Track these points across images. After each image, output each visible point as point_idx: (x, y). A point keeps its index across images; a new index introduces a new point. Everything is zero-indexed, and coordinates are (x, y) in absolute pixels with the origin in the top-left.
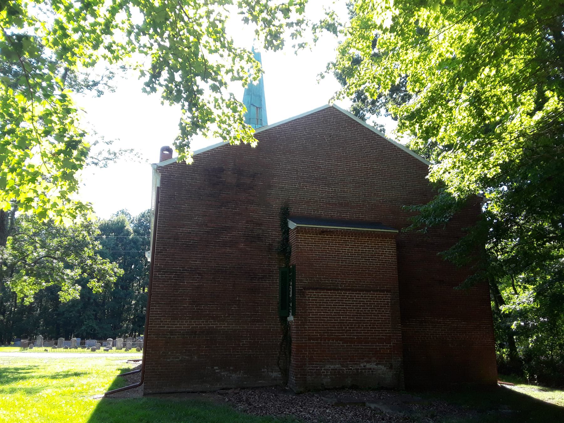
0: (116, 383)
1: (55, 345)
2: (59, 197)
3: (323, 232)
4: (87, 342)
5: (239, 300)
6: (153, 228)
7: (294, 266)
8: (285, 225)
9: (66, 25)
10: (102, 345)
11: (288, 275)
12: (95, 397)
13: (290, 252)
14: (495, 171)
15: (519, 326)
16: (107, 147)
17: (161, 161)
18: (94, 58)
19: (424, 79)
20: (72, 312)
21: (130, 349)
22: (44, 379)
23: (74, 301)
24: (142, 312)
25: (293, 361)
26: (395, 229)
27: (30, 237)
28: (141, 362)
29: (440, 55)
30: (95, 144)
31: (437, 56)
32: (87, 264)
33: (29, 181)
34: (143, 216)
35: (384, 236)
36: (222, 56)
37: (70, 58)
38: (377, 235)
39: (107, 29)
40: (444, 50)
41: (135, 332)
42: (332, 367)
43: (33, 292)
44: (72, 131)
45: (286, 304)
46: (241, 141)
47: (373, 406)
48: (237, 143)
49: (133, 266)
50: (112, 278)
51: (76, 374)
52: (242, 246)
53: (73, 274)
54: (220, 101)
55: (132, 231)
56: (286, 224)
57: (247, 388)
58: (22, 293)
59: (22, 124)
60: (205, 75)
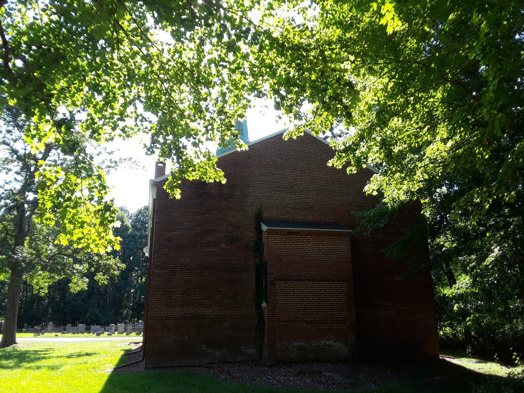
0: (122, 360)
1: (64, 331)
2: (96, 236)
3: (289, 233)
4: (92, 327)
5: (222, 290)
6: (150, 232)
7: (266, 262)
8: (259, 227)
9: (94, 116)
10: (105, 331)
11: (261, 269)
12: (106, 371)
13: (263, 250)
14: (418, 186)
15: (459, 308)
16: (109, 157)
17: (156, 178)
18: (112, 135)
19: (356, 119)
20: (77, 300)
21: (131, 333)
22: (62, 359)
23: (81, 292)
24: (140, 300)
25: (266, 341)
26: (350, 229)
27: (44, 237)
28: (141, 344)
29: (367, 103)
30: (98, 155)
31: (364, 104)
32: (94, 261)
33: (80, 227)
34: (140, 212)
35: (340, 235)
36: (199, 124)
37: (97, 137)
38: (334, 235)
39: (122, 116)
40: (370, 99)
41: (134, 318)
42: (298, 344)
43: (47, 284)
44: (107, 199)
45: (261, 293)
46: (215, 180)
47: (327, 374)
48: (212, 181)
49: (131, 258)
50: (116, 272)
51: (87, 354)
52: (223, 245)
53: (81, 268)
54: (199, 153)
55: (130, 226)
56: (260, 226)
57: (229, 362)
58: (37, 285)
59: (75, 194)
60: (189, 136)
